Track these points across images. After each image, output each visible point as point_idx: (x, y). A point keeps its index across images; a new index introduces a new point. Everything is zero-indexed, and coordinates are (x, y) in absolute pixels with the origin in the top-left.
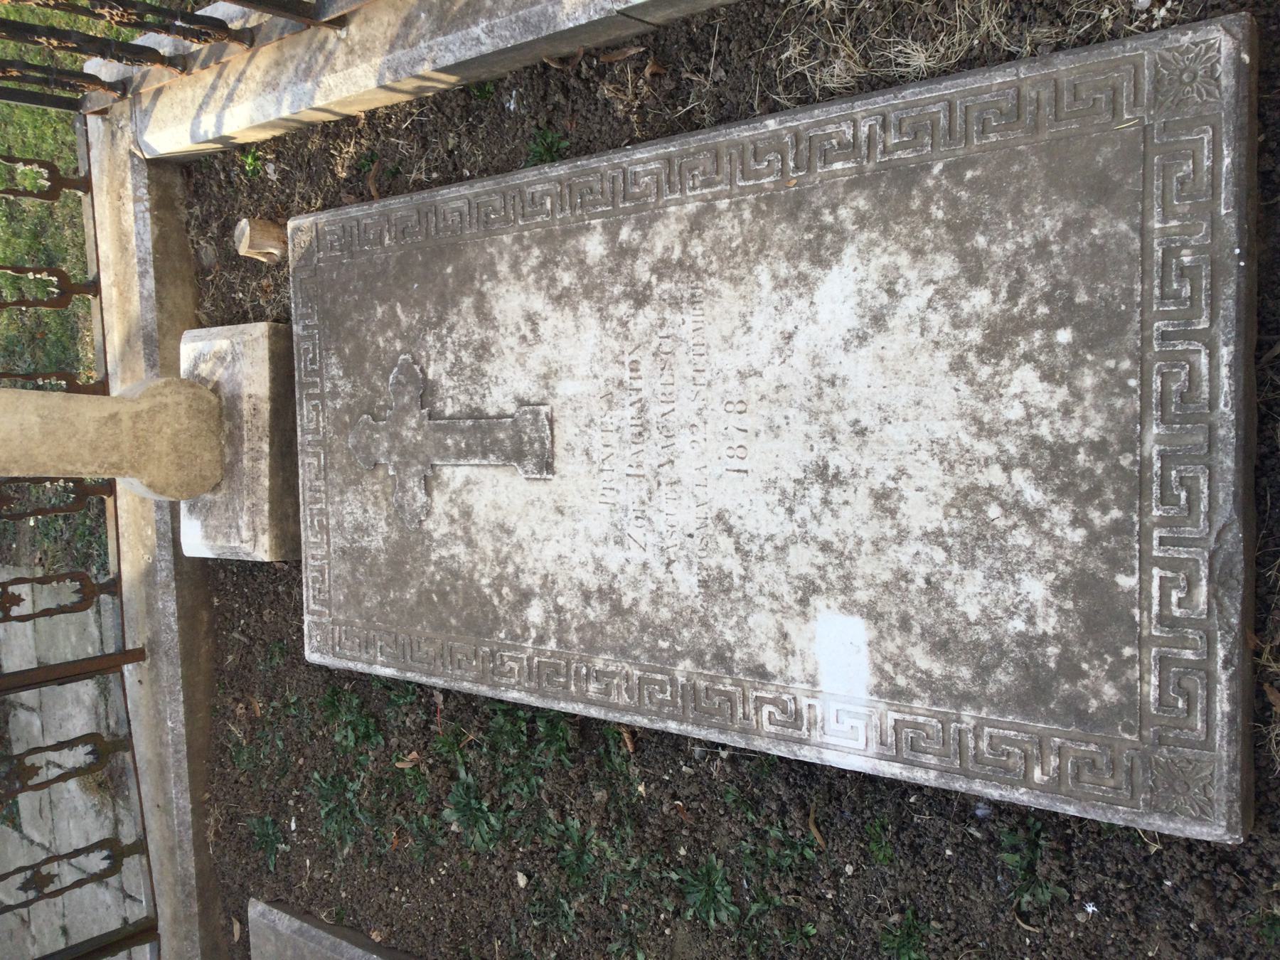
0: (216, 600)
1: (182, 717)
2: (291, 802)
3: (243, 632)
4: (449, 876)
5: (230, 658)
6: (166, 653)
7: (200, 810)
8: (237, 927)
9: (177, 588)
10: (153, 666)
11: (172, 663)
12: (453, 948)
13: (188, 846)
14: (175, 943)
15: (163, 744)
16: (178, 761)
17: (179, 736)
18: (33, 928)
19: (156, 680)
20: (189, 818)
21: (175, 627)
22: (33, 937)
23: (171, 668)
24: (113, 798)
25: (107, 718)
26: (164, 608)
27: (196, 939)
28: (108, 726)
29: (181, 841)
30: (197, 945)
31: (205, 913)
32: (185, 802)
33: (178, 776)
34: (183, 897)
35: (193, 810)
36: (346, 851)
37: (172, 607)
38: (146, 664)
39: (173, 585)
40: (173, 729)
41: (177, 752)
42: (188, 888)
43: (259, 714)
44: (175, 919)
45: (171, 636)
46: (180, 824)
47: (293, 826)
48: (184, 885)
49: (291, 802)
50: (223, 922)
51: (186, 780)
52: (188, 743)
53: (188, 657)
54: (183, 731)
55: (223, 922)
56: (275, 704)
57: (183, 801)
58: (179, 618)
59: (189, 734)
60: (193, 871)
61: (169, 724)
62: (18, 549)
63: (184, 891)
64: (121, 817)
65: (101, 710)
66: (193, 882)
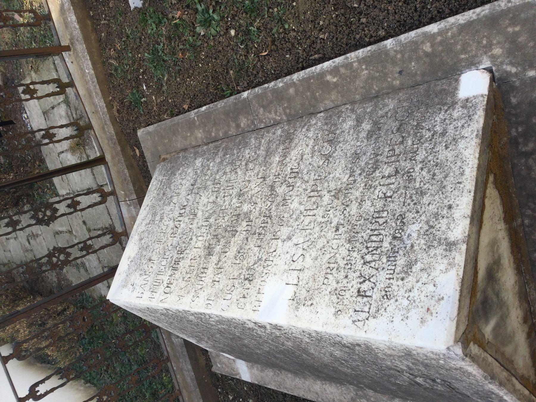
0: (91, 12)
1: (91, 66)
2: (141, 77)
3: (105, 20)
4: (206, 57)
5: (103, 34)
6: (78, 41)
7: (109, 106)
8: (137, 151)
9: (74, 9)
10: (75, 50)
11: (81, 44)
12: (215, 89)
13: (109, 123)
14: (115, 168)
15: (87, 83)
16: (95, 86)
17: (91, 75)
18: (74, 233)
19: (77, 57)
20: (106, 110)
21: (77, 27)
22: (75, 236)
23: (81, 46)
24: (84, 147)
25: (72, 115)
26: (71, 20)
27: (123, 161)
28: (73, 118)
29: (105, 121)
30: (124, 164)
31: (123, 150)
32: (102, 104)
33: (96, 93)
34: (112, 145)
35: (106, 106)
36: (165, 79)
37: (74, 18)
38: (71, 53)
39: (72, 8)
40: (89, 73)
41: (93, 82)
42: (114, 141)
43: (119, 49)
44: (113, 158)
45: (77, 32)
46: (103, 114)
47: (145, 88)
48: (112, 140)
49: (141, 77)
50: (132, 153)
51: (100, 94)
52: (96, 77)
53: (86, 39)
54: (93, 72)
55: (132, 153)
56: (124, 39)
57: (100, 102)
58: (78, 22)
59: (96, 73)
60: (113, 132)
61: (87, 71)
62: (23, 71)
63: (112, 142)
64: (89, 154)
65: (70, 113)
66: (115, 137)
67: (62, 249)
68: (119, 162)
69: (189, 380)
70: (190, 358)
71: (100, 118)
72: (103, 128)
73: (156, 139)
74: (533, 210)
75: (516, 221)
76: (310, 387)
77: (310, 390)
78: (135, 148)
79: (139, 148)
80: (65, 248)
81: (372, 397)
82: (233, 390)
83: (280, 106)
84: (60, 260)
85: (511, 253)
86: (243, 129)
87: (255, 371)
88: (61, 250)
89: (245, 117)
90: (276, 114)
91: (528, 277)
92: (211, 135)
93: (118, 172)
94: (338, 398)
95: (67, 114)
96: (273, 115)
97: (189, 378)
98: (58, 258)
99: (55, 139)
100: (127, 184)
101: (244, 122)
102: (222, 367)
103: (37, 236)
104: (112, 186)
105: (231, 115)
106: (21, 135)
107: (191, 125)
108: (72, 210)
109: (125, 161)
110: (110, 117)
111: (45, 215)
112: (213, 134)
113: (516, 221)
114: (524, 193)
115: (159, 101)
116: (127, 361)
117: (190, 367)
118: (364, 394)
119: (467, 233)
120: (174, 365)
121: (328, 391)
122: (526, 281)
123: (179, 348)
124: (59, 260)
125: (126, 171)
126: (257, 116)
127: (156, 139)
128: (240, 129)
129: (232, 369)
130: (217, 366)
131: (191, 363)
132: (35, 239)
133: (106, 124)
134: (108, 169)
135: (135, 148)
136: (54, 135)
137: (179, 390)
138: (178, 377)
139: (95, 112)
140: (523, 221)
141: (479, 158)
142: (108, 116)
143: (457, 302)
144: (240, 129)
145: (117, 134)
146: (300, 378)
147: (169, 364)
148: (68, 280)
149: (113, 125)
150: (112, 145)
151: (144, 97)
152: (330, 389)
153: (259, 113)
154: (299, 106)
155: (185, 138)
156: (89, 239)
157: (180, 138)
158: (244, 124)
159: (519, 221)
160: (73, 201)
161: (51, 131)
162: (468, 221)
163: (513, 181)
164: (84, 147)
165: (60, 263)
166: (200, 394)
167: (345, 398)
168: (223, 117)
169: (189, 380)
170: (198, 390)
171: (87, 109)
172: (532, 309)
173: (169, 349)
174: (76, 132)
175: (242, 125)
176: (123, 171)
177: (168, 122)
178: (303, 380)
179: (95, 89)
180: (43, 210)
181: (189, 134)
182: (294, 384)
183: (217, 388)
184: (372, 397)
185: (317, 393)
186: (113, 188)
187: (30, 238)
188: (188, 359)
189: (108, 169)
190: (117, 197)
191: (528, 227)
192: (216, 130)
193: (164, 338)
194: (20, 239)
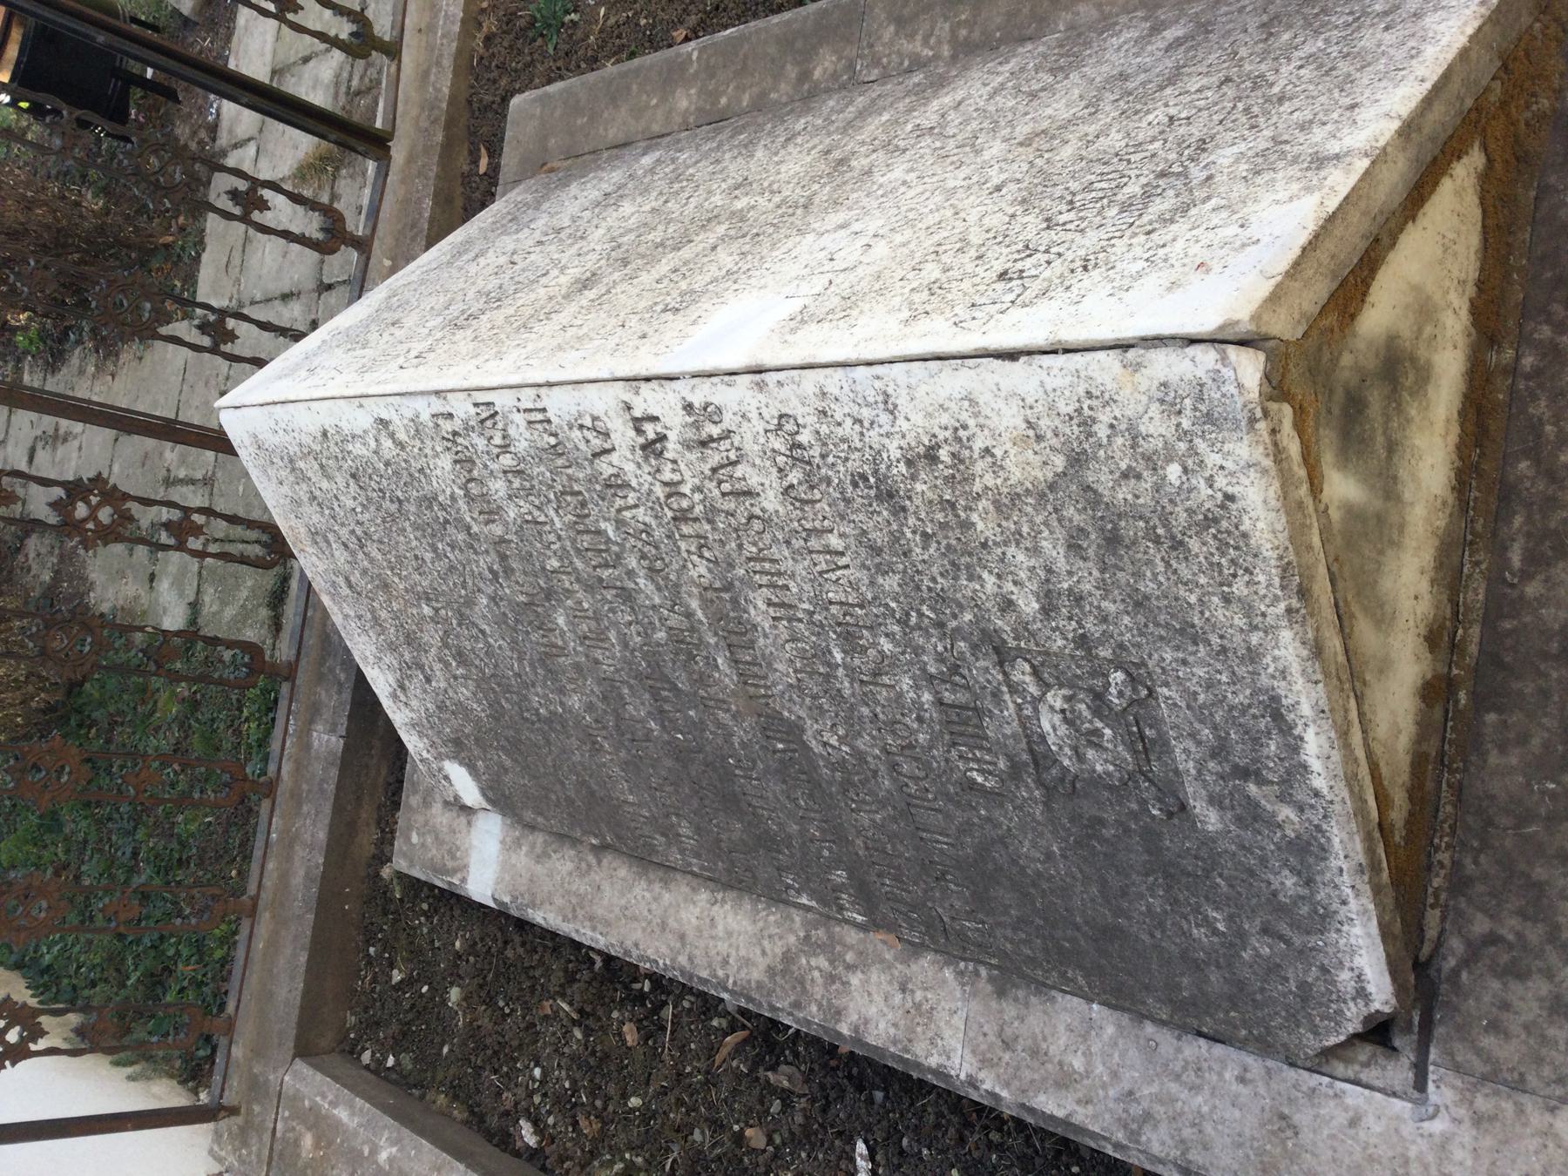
13: (447, 62)
20: (457, 28)
27: (432, 174)
31: (448, 147)
35: (463, 21)
44: (411, 159)
46: (443, 36)
60: (446, 91)
65: (345, 75)
66: (444, 105)
67: (117, 495)
68: (420, 174)
69: (298, 879)
70: (338, 809)
71: (430, 48)
72: (426, 74)
73: (558, 113)
74: (1560, 328)
75: (1498, 353)
76: (672, 911)
77: (663, 926)
78: (483, 150)
79: (495, 152)
80: (126, 497)
81: (851, 947)
82: (415, 953)
83: (946, 19)
84: (95, 519)
85: (1459, 413)
86: (816, 85)
87: (521, 859)
88: (114, 496)
89: (835, 52)
90: (926, 42)
91: (1479, 527)
92: (715, 103)
93: (406, 201)
94: (743, 953)
95: (338, 76)
96: (918, 44)
97: (302, 873)
98: (93, 510)
99: (227, 348)
100: (413, 239)
101: (827, 64)
102: (423, 845)
103: (65, 440)
104: (370, 224)
105: (799, 45)
106: (180, 153)
107: (674, 76)
108: (237, 211)
109: (437, 176)
110: (459, 51)
111: (93, 510)
112: (724, 101)
113: (1498, 353)
114: (1549, 275)
115: (612, 21)
116: (128, 854)
117: (322, 836)
118: (831, 936)
119: (1382, 143)
120: (275, 824)
121: (720, 927)
122: (1469, 537)
123: (317, 768)
124: (93, 516)
125: (428, 203)
126: (871, 46)
127: (558, 113)
128: (806, 87)
129: (450, 852)
130: (408, 839)
131: (331, 826)
132: (54, 449)
133: (438, 64)
134: (383, 173)
135: (483, 150)
136: (232, 336)
137: (255, 900)
138: (271, 866)
139: (427, 30)
140: (1518, 358)
141: (1471, 37)
142: (455, 45)
143: (1297, 251)
144: (806, 87)
145: (452, 100)
146: (650, 882)
147: (285, 688)
148: (83, 579)
149: (456, 73)
150: (424, 124)
151: (575, 11)
152: (730, 919)
153: (879, 38)
154: (998, 20)
155: (637, 113)
156: (200, 510)
157: (623, 111)
158: (825, 70)
159: (1509, 354)
160: (253, 189)
161: (231, 323)
162: (1396, 124)
163: (1528, 236)
164: (337, 169)
165: (91, 526)
166: (309, 933)
167: (764, 953)
168: (772, 50)
169: (298, 879)
170: (311, 917)
171: (407, 21)
172: (1460, 632)
173: (267, 883)
174: (320, 236)
175: (817, 74)
176: (419, 201)
177: (610, 69)
178: (657, 887)
179: (273, 943)
180: (94, 500)
181: (654, 101)
182: (623, 902)
183: (368, 943)
184: (851, 947)
185: (682, 937)
186: (368, 232)
187: (40, 445)
188: (327, 809)
189: (383, 173)
190: (368, 259)
191: (1528, 377)
192: (737, 88)
193: (291, 730)
194: (9, 449)
